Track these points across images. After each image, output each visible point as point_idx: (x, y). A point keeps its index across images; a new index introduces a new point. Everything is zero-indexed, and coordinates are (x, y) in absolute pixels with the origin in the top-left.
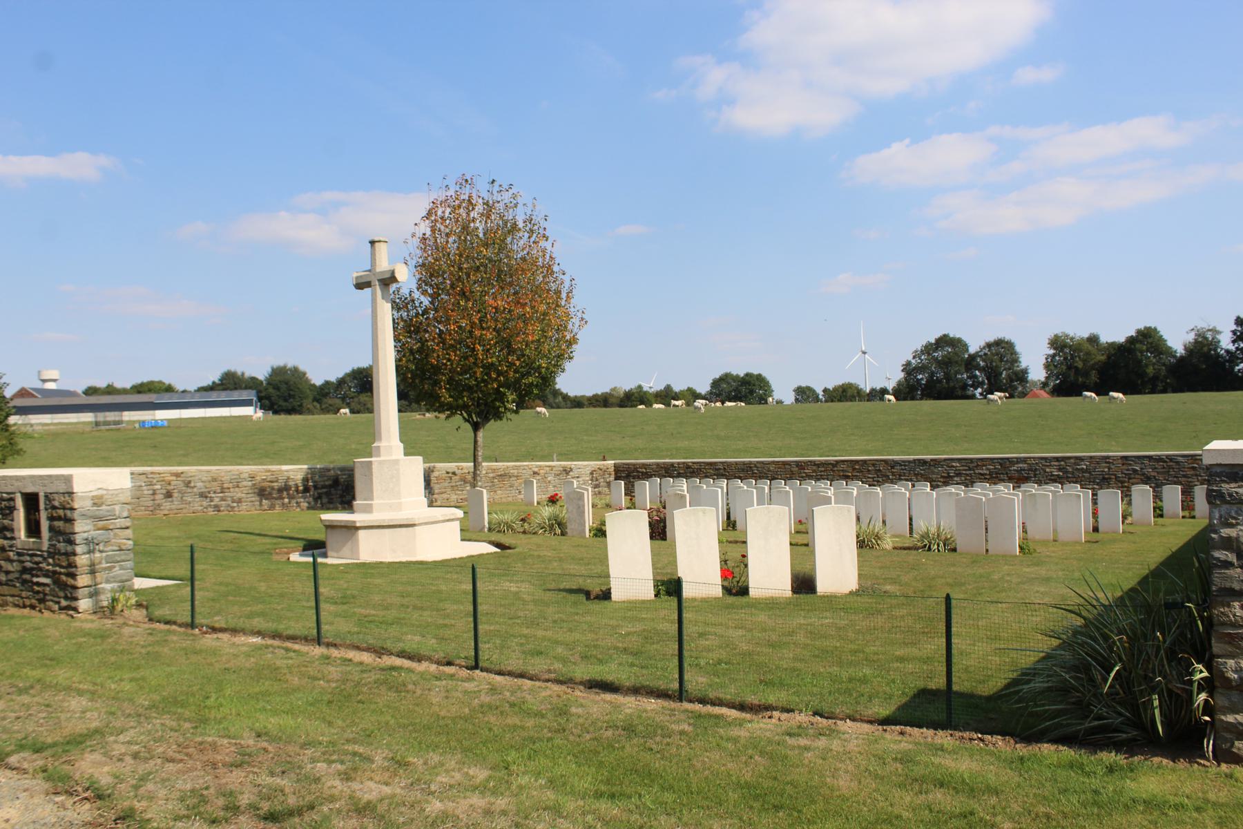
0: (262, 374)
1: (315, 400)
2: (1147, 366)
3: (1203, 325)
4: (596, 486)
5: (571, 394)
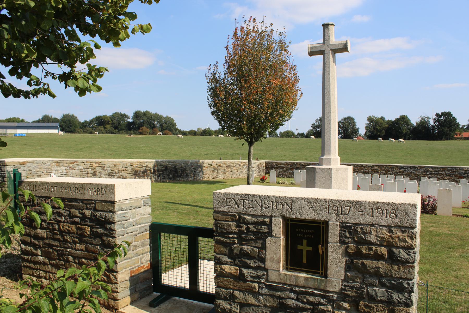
0: (59, 117)
1: (81, 128)
2: (403, 129)
3: (424, 115)
4: (259, 172)
5: (182, 130)
